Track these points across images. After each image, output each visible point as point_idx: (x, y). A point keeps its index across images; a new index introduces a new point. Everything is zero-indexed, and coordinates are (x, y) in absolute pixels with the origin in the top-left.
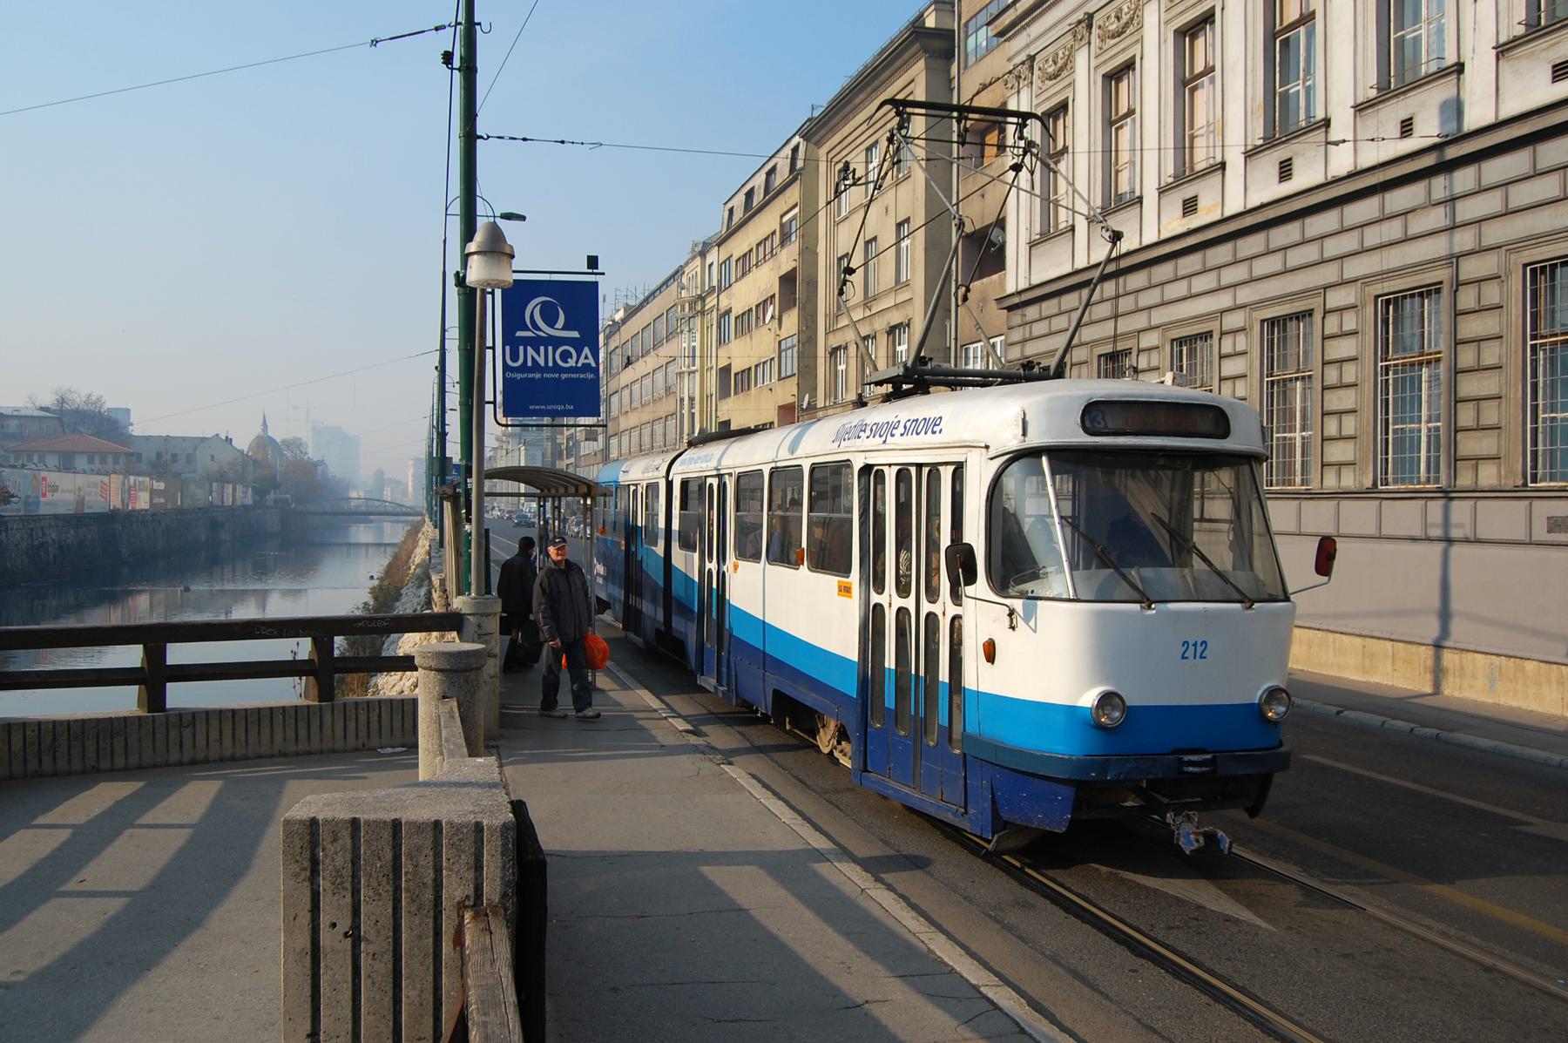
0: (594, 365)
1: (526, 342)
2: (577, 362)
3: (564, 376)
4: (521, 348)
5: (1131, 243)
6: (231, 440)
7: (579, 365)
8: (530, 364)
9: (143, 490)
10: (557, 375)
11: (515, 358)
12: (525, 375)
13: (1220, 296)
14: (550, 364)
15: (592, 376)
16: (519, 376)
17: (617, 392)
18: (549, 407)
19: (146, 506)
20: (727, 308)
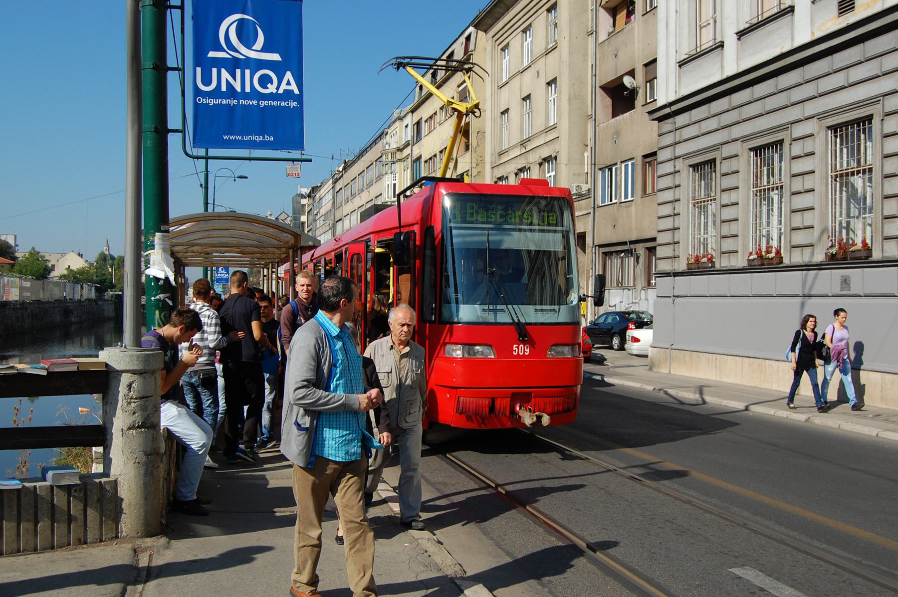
0: (297, 92)
1: (219, 63)
2: (278, 88)
3: (263, 103)
4: (214, 70)
5: (783, 47)
6: (82, 255)
7: (281, 91)
8: (224, 88)
9: (14, 287)
10: (255, 102)
11: (207, 81)
12: (218, 101)
13: (882, 81)
14: (248, 90)
15: (295, 104)
16: (212, 102)
17: (341, 219)
18: (246, 138)
19: (17, 298)
20: (418, 156)
